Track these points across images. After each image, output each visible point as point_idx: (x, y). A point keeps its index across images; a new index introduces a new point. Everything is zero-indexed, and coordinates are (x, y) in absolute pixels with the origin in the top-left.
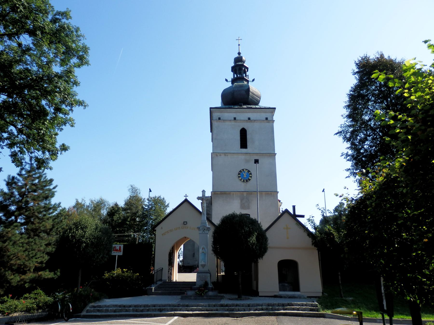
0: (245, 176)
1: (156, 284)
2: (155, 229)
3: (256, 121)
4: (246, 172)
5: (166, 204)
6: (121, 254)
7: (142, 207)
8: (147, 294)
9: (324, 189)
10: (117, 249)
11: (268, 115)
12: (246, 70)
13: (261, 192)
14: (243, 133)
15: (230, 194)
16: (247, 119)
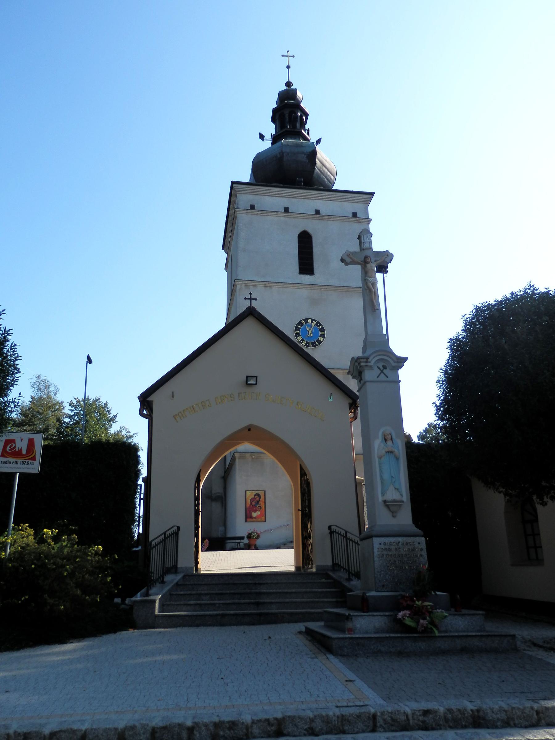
0: (310, 334)
1: (163, 582)
2: (149, 399)
4: (313, 326)
5: (111, 416)
6: (35, 467)
7: (59, 420)
8: (134, 626)
10: (20, 451)
11: (357, 207)
12: (304, 117)
16: (314, 213)
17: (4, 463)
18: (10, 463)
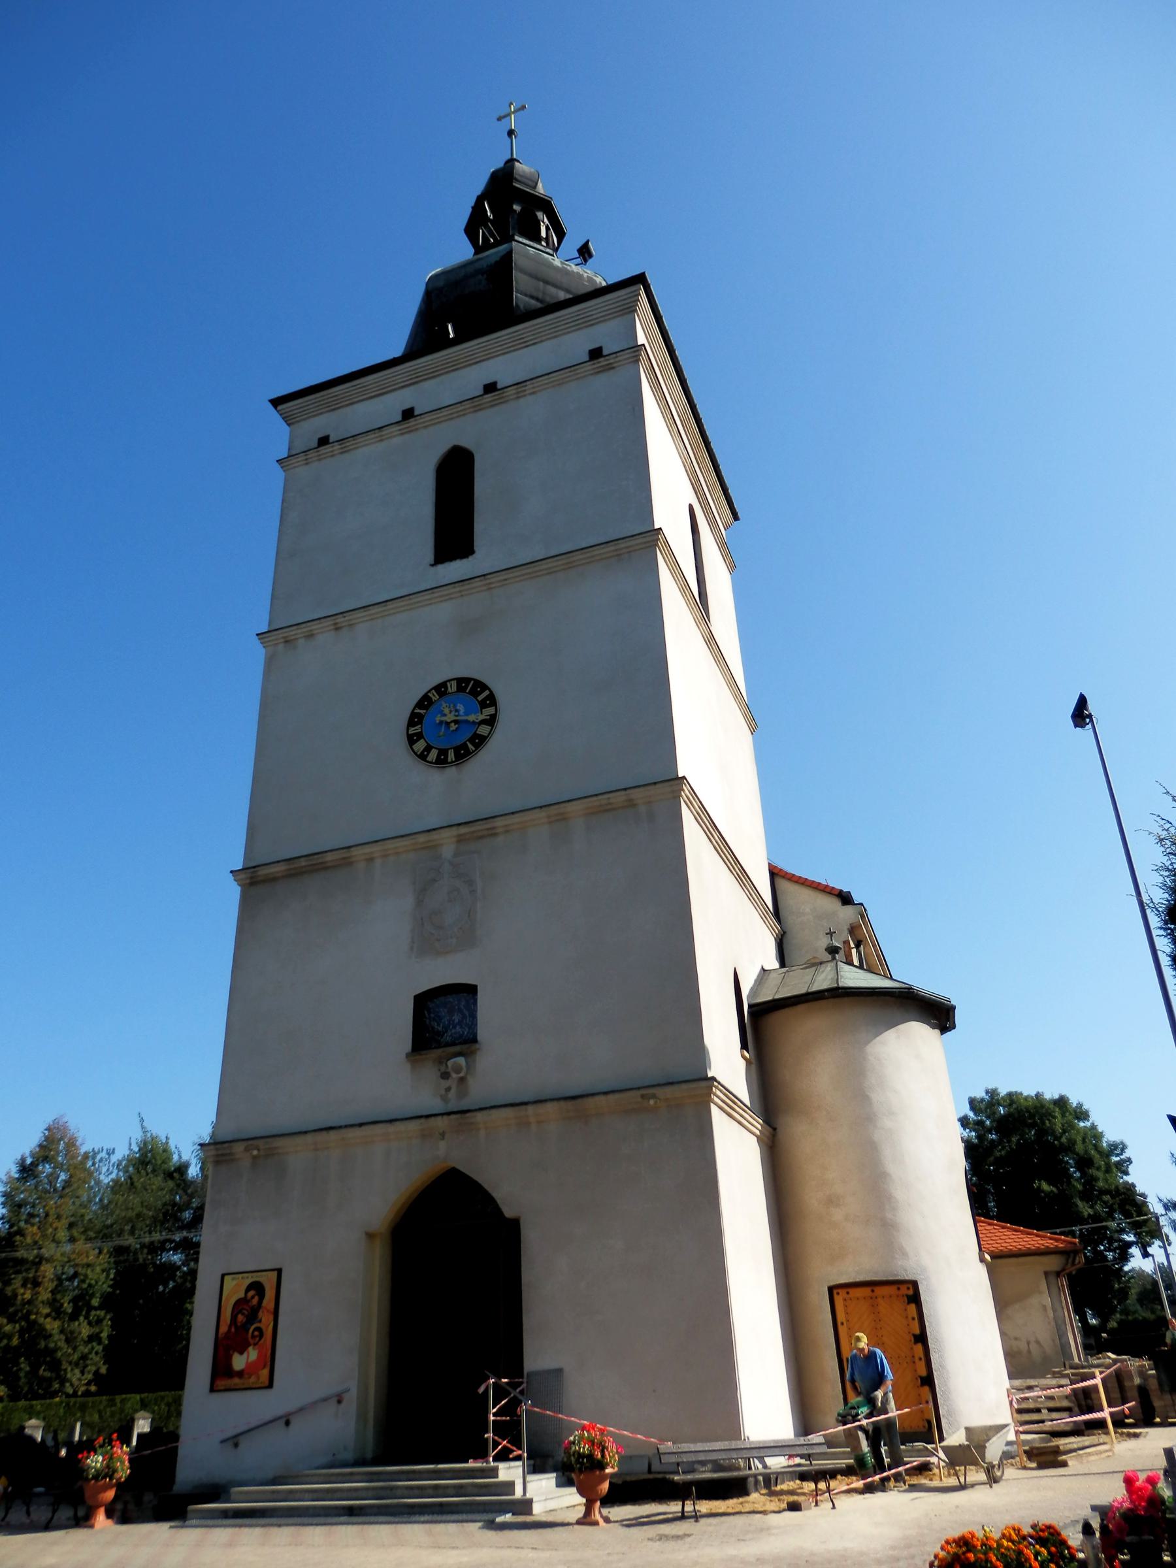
3: (529, 385)
13: (553, 810)
15: (347, 863)
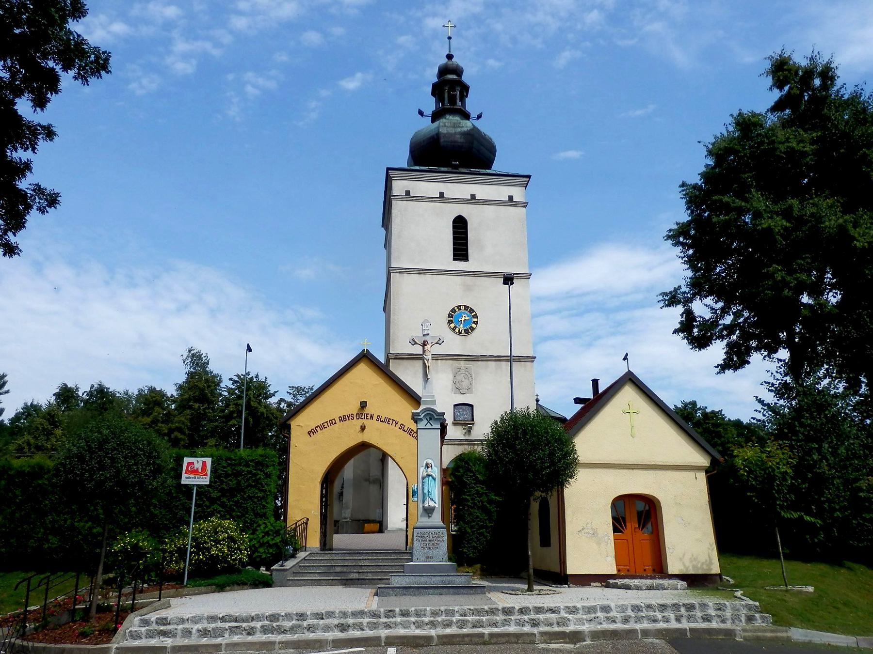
2: (288, 423)
6: (206, 481)
9: (627, 355)
14: (460, 225)
17: (187, 478)
18: (191, 478)
